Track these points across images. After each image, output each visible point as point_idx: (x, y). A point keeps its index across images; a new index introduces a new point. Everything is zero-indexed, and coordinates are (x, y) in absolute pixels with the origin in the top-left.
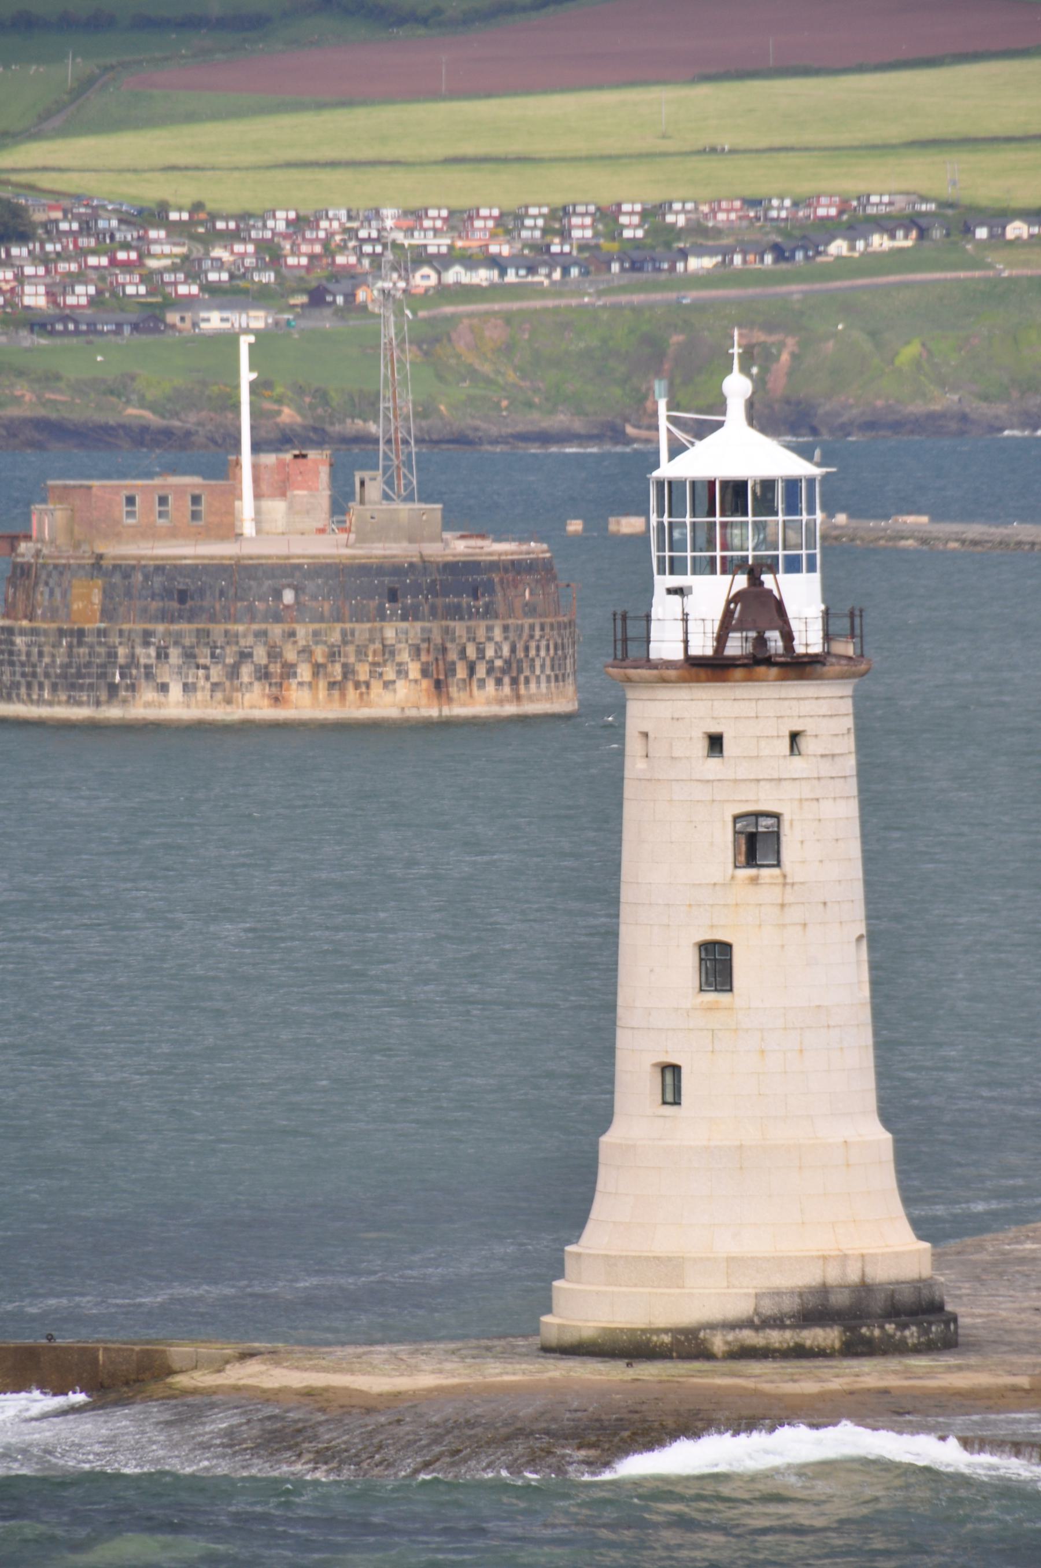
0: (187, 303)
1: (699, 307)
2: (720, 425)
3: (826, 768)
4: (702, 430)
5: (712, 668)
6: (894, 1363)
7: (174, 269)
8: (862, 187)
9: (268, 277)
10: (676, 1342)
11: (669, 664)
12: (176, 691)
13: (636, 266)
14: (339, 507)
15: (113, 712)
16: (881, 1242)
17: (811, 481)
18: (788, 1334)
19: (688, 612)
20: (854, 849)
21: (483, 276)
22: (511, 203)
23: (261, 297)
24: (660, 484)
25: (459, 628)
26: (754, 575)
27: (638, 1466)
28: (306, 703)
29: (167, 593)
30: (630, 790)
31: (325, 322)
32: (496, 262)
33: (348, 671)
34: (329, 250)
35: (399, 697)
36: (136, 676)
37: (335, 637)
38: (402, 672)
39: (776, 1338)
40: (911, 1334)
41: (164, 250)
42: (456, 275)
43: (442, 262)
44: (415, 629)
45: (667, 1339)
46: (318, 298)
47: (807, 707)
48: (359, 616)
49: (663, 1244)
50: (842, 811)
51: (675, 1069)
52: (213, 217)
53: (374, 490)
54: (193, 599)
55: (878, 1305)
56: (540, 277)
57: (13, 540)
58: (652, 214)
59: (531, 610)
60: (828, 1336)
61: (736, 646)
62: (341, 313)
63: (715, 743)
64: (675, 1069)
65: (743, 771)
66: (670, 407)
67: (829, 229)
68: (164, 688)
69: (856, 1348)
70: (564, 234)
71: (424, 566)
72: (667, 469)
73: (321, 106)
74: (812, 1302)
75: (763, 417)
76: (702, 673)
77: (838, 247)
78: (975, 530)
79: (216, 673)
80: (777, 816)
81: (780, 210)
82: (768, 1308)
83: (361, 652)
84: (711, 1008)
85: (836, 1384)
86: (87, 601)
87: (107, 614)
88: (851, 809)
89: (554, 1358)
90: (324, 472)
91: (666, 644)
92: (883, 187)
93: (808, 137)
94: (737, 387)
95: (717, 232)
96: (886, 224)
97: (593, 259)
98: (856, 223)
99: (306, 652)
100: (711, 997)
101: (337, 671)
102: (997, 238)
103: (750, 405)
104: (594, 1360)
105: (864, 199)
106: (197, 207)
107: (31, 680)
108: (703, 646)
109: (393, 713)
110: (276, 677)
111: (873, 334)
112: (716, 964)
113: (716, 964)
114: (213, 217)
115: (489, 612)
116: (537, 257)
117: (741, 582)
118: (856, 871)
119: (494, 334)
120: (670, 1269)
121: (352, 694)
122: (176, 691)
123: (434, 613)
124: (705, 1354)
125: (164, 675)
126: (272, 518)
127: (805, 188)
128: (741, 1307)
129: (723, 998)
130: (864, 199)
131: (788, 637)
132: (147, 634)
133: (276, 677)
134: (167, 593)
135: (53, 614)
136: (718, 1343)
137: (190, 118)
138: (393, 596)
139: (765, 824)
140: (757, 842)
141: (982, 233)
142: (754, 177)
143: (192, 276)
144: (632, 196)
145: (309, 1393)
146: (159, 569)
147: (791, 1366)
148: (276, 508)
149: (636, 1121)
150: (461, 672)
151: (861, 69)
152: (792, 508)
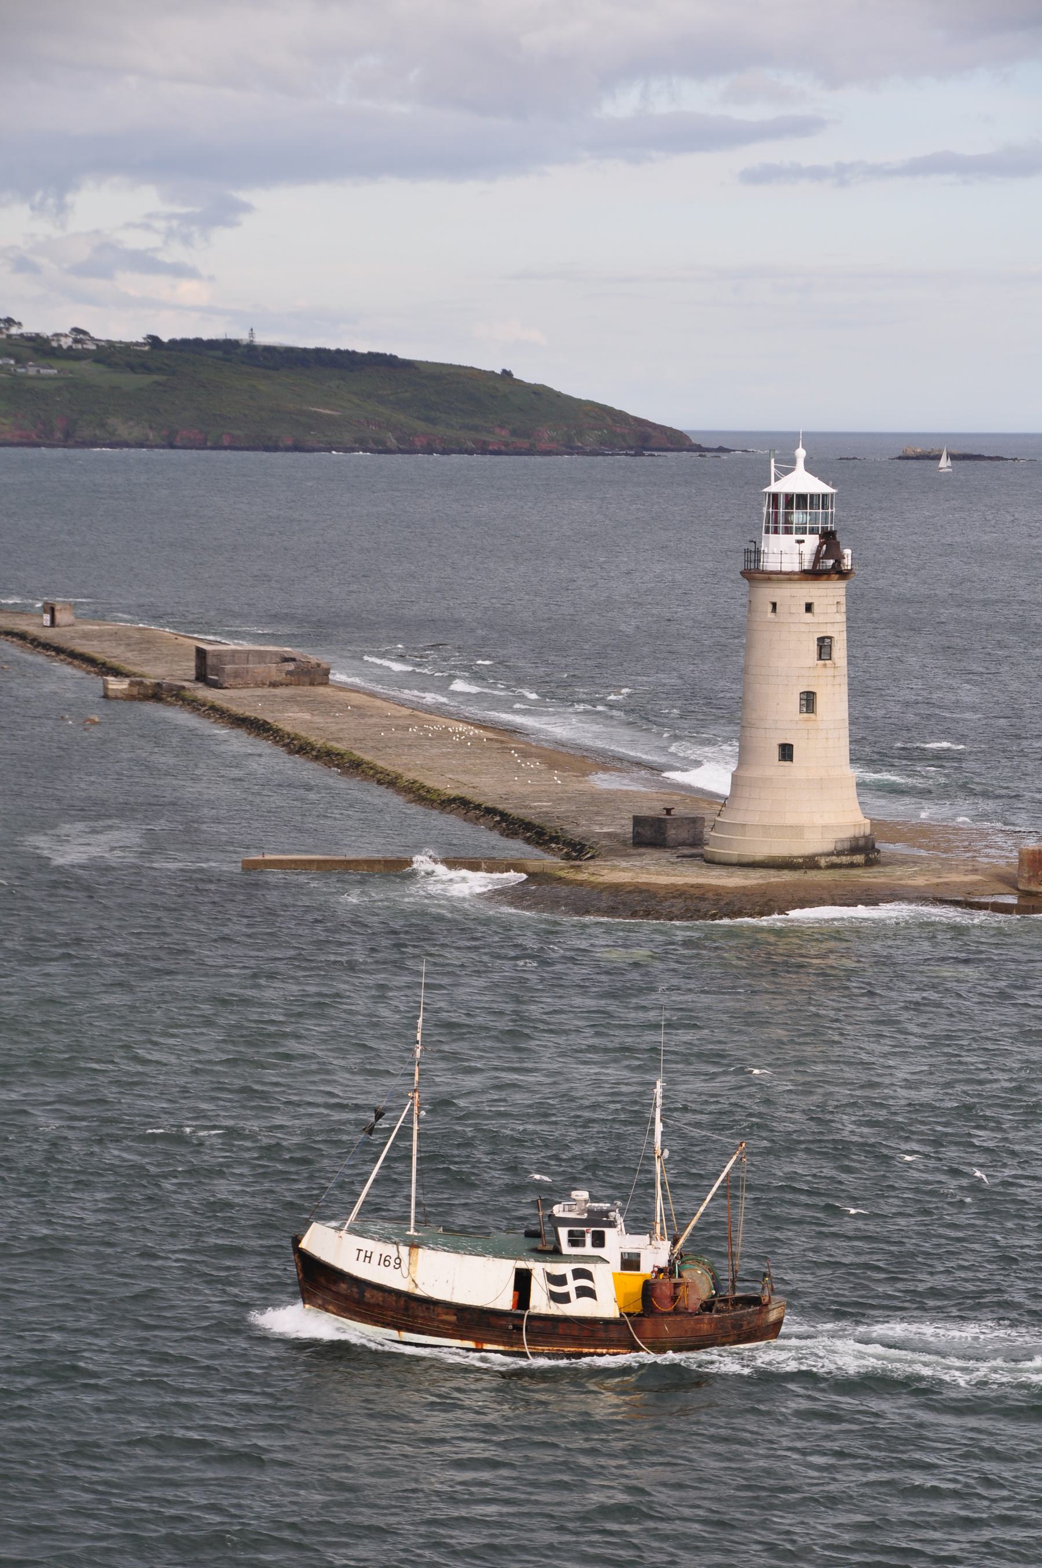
2: (793, 470)
4: (787, 472)
5: (814, 574)
10: (805, 862)
17: (832, 495)
18: (849, 858)
19: (788, 551)
39: (845, 859)
45: (801, 860)
49: (790, 820)
60: (859, 858)
63: (809, 608)
66: (776, 462)
72: (774, 487)
75: (811, 467)
76: (810, 577)
80: (830, 638)
82: (840, 847)
89: (697, 865)
104: (761, 870)
108: (807, 566)
120: (797, 830)
124: (817, 867)
128: (829, 847)
136: (823, 862)
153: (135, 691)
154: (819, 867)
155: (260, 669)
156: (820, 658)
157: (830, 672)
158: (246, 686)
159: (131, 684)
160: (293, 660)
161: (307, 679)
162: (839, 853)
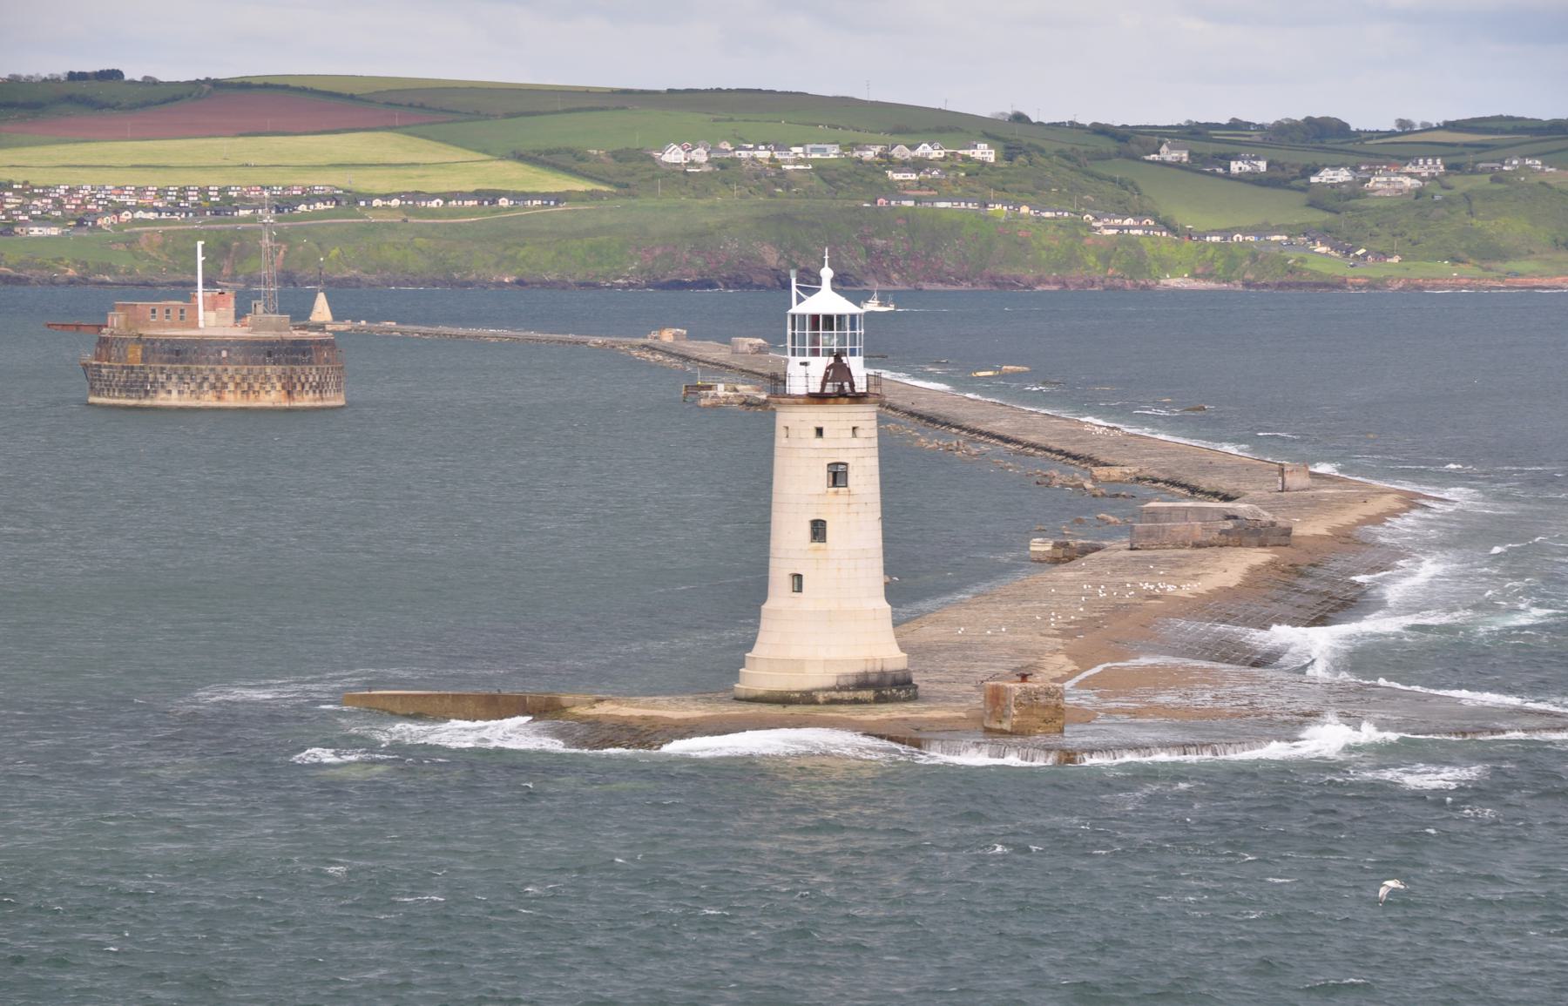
0: (23, 223)
1: (244, 231)
3: (867, 443)
4: (811, 292)
5: (819, 398)
6: (899, 706)
7: (17, 209)
8: (310, 183)
9: (58, 213)
11: (799, 396)
12: (175, 393)
13: (217, 213)
14: (239, 315)
15: (147, 402)
16: (886, 653)
19: (806, 374)
20: (877, 479)
21: (152, 215)
22: (162, 185)
23: (55, 222)
24: (793, 316)
25: (298, 368)
26: (838, 357)
27: (676, 747)
28: (232, 400)
29: (171, 351)
30: (777, 452)
31: (84, 233)
32: (156, 210)
33: (250, 386)
34: (84, 203)
35: (272, 398)
36: (158, 386)
37: (245, 372)
38: (273, 387)
39: (846, 695)
40: (902, 693)
41: (12, 201)
42: (140, 214)
43: (134, 209)
44: (279, 368)
46: (80, 223)
47: (860, 416)
48: (255, 362)
49: (794, 653)
50: (873, 463)
51: (799, 577)
52: (33, 188)
53: (260, 309)
54: (184, 355)
55: (889, 680)
56: (176, 217)
57: (100, 327)
58: (223, 191)
59: (327, 361)
60: (868, 694)
61: (829, 389)
62: (90, 229)
63: (819, 432)
64: (799, 577)
65: (833, 444)
67: (298, 200)
68: (169, 392)
69: (880, 699)
70: (185, 199)
71: (282, 342)
72: (796, 309)
73: (76, 142)
74: (862, 679)
77: (302, 208)
78: (423, 329)
79: (193, 386)
81: (277, 191)
82: (842, 682)
83: (256, 378)
84: (817, 550)
85: (883, 716)
86: (135, 354)
87: (144, 359)
88: (875, 462)
90: (232, 300)
91: (796, 386)
92: (321, 182)
93: (287, 161)
94: (827, 273)
95: (251, 200)
96: (323, 199)
97: (198, 210)
98: (309, 198)
99: (232, 377)
100: (816, 544)
101: (245, 386)
102: (369, 205)
103: (833, 281)
105: (312, 188)
106: (26, 183)
107: (109, 387)
108: (816, 389)
109: (270, 405)
110: (219, 388)
111: (319, 244)
112: (818, 530)
113: (818, 530)
114: (33, 188)
115: (310, 362)
116: (174, 208)
117: (832, 360)
118: (877, 489)
119: (157, 240)
120: (799, 664)
121: (252, 396)
122: (175, 393)
123: (287, 362)
125: (170, 386)
126: (212, 319)
127: (287, 182)
128: (830, 681)
129: (822, 545)
130: (312, 188)
131: (852, 385)
132: (162, 369)
133: (219, 388)
134: (171, 351)
135: (119, 359)
136: (821, 697)
137: (20, 145)
138: (269, 354)
139: (841, 467)
140: (838, 475)
141: (362, 203)
142: (202, 179)
143: (25, 213)
144: (214, 182)
145: (644, 718)
146: (167, 341)
147: (857, 708)
148: (212, 315)
149: (779, 598)
150: (299, 388)
151: (306, 133)
152: (853, 328)
153: (1060, 553)
154: (817, 703)
155: (1180, 527)
156: (835, 484)
157: (843, 499)
158: (1163, 546)
159: (1056, 546)
160: (1235, 517)
161: (1253, 540)
162: (841, 689)
